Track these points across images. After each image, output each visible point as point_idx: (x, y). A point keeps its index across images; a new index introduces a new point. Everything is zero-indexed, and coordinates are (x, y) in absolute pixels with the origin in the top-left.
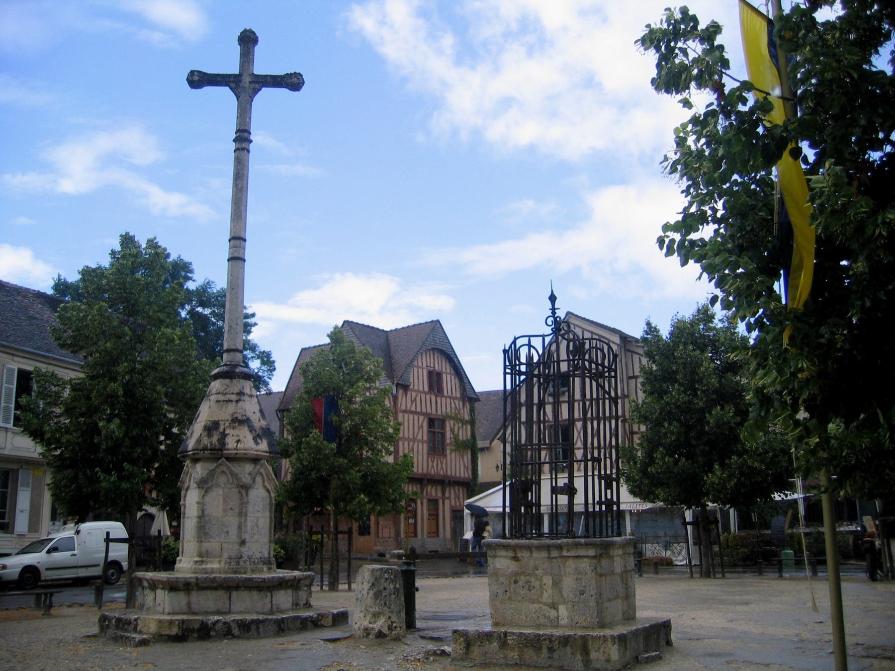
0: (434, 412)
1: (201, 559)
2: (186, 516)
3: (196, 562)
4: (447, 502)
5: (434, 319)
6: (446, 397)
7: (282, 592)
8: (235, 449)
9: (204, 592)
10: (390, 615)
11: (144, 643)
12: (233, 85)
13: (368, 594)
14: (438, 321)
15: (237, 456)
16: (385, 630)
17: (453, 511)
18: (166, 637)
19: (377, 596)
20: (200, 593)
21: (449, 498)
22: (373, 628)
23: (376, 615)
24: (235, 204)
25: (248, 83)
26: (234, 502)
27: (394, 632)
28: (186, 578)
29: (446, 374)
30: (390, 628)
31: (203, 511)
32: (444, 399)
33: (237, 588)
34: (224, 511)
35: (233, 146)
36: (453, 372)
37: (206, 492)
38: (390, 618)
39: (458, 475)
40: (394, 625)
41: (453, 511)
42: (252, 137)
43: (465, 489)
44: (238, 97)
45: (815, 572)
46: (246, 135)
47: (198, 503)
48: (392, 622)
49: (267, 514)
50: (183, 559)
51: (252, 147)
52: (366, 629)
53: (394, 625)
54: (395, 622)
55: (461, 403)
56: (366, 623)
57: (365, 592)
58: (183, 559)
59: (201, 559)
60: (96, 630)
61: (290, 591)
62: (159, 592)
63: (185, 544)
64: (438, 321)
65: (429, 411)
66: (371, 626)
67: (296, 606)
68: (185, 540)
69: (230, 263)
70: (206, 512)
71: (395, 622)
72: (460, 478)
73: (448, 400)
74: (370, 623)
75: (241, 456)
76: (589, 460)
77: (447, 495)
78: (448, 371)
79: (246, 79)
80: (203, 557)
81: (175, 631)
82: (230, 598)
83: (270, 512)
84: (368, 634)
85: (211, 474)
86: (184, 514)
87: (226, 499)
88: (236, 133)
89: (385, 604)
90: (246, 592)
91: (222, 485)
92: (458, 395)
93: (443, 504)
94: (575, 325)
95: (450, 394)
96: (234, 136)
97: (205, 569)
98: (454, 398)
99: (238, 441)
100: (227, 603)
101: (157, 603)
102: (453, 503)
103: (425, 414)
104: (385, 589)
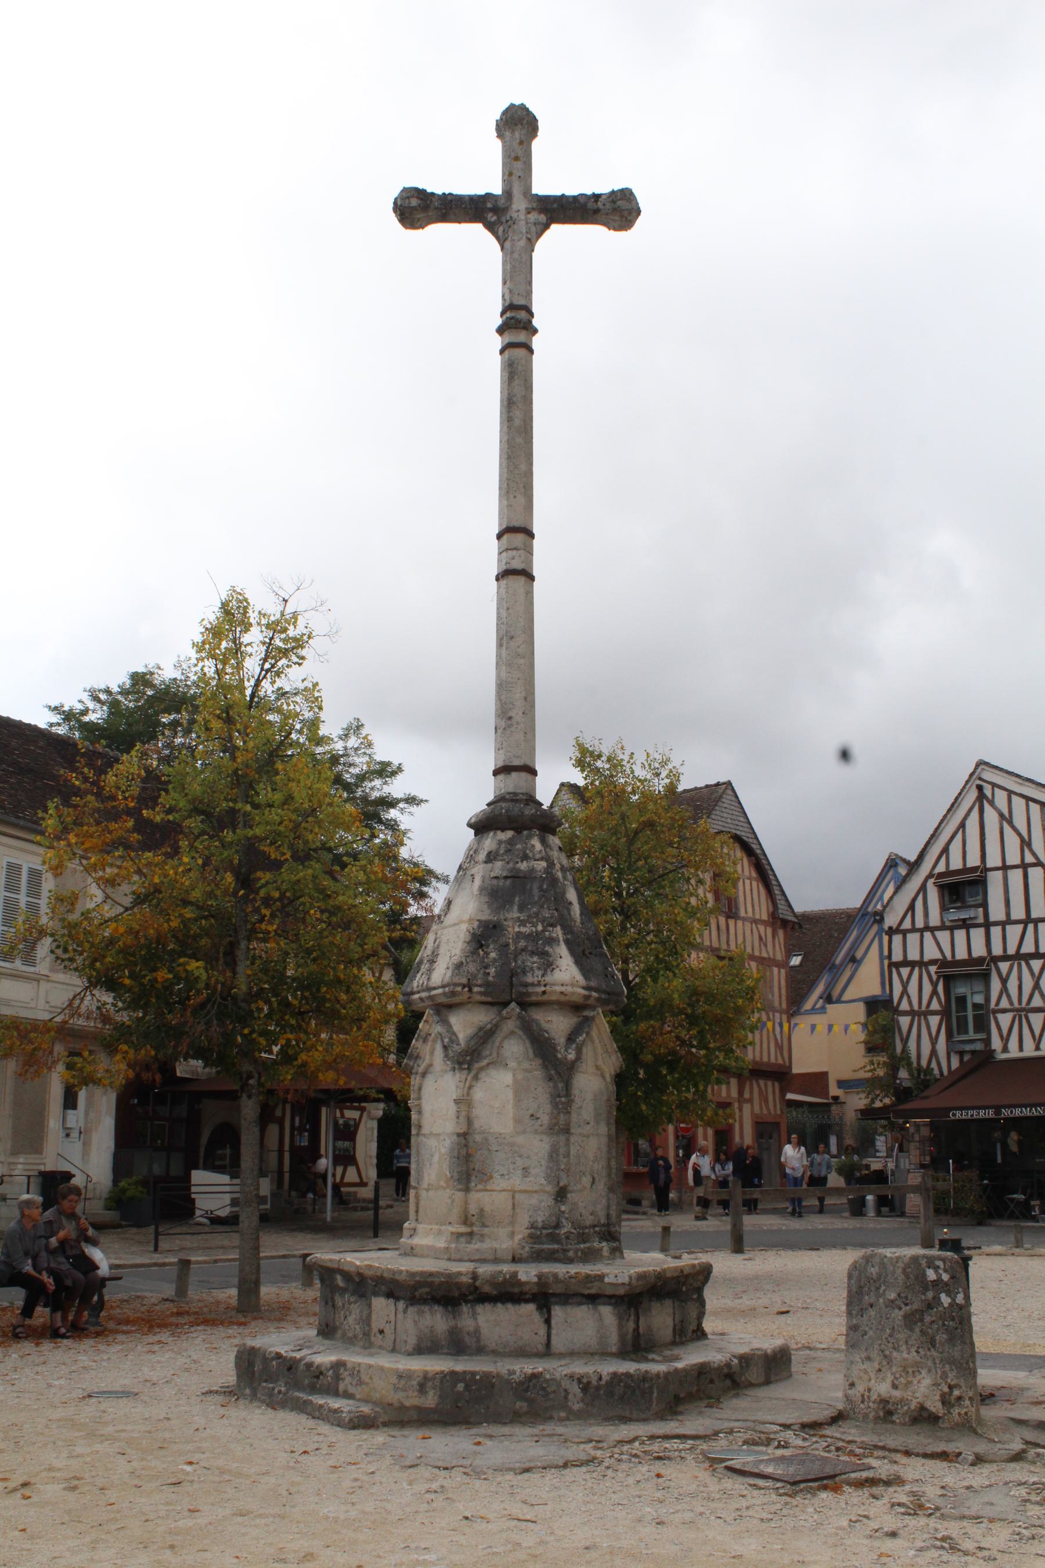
0: (724, 946)
2: (425, 1131)
3: (459, 1235)
4: (747, 1108)
5: (722, 780)
6: (744, 919)
7: (656, 1306)
11: (362, 1423)
12: (492, 217)
14: (729, 784)
16: (935, 1405)
17: (756, 1123)
20: (479, 1308)
21: (750, 1101)
22: (902, 1401)
24: (509, 458)
25: (523, 212)
26: (540, 1099)
27: (956, 1411)
28: (450, 1276)
29: (750, 878)
30: (945, 1401)
31: (469, 1121)
32: (740, 923)
34: (517, 1121)
35: (497, 342)
36: (754, 874)
37: (476, 1078)
39: (765, 1059)
40: (956, 1392)
41: (756, 1123)
42: (535, 322)
43: (777, 1085)
44: (502, 241)
46: (522, 315)
47: (457, 1102)
48: (950, 1387)
49: (603, 1129)
50: (421, 1227)
51: (536, 342)
52: (884, 1402)
53: (956, 1392)
54: (956, 1386)
55: (769, 930)
58: (421, 1227)
60: (230, 1377)
61: (668, 1302)
62: (380, 1304)
63: (423, 1194)
64: (729, 784)
65: (715, 944)
66: (897, 1394)
67: (680, 1335)
68: (425, 1185)
69: (503, 582)
70: (477, 1124)
71: (956, 1386)
72: (768, 1064)
73: (748, 925)
74: (895, 1387)
75: (554, 998)
77: (747, 1095)
78: (747, 873)
79: (519, 204)
80: (472, 1225)
81: (430, 1400)
82: (548, 1321)
83: (608, 1124)
84: (890, 1413)
85: (485, 1036)
86: (420, 1127)
87: (519, 1091)
88: (502, 314)
90: (584, 1308)
91: (512, 1064)
92: (765, 917)
93: (741, 1110)
94: (994, 785)
95: (750, 914)
96: (499, 321)
98: (755, 921)
100: (542, 1331)
101: (376, 1325)
102: (757, 1110)
104: (930, 1306)
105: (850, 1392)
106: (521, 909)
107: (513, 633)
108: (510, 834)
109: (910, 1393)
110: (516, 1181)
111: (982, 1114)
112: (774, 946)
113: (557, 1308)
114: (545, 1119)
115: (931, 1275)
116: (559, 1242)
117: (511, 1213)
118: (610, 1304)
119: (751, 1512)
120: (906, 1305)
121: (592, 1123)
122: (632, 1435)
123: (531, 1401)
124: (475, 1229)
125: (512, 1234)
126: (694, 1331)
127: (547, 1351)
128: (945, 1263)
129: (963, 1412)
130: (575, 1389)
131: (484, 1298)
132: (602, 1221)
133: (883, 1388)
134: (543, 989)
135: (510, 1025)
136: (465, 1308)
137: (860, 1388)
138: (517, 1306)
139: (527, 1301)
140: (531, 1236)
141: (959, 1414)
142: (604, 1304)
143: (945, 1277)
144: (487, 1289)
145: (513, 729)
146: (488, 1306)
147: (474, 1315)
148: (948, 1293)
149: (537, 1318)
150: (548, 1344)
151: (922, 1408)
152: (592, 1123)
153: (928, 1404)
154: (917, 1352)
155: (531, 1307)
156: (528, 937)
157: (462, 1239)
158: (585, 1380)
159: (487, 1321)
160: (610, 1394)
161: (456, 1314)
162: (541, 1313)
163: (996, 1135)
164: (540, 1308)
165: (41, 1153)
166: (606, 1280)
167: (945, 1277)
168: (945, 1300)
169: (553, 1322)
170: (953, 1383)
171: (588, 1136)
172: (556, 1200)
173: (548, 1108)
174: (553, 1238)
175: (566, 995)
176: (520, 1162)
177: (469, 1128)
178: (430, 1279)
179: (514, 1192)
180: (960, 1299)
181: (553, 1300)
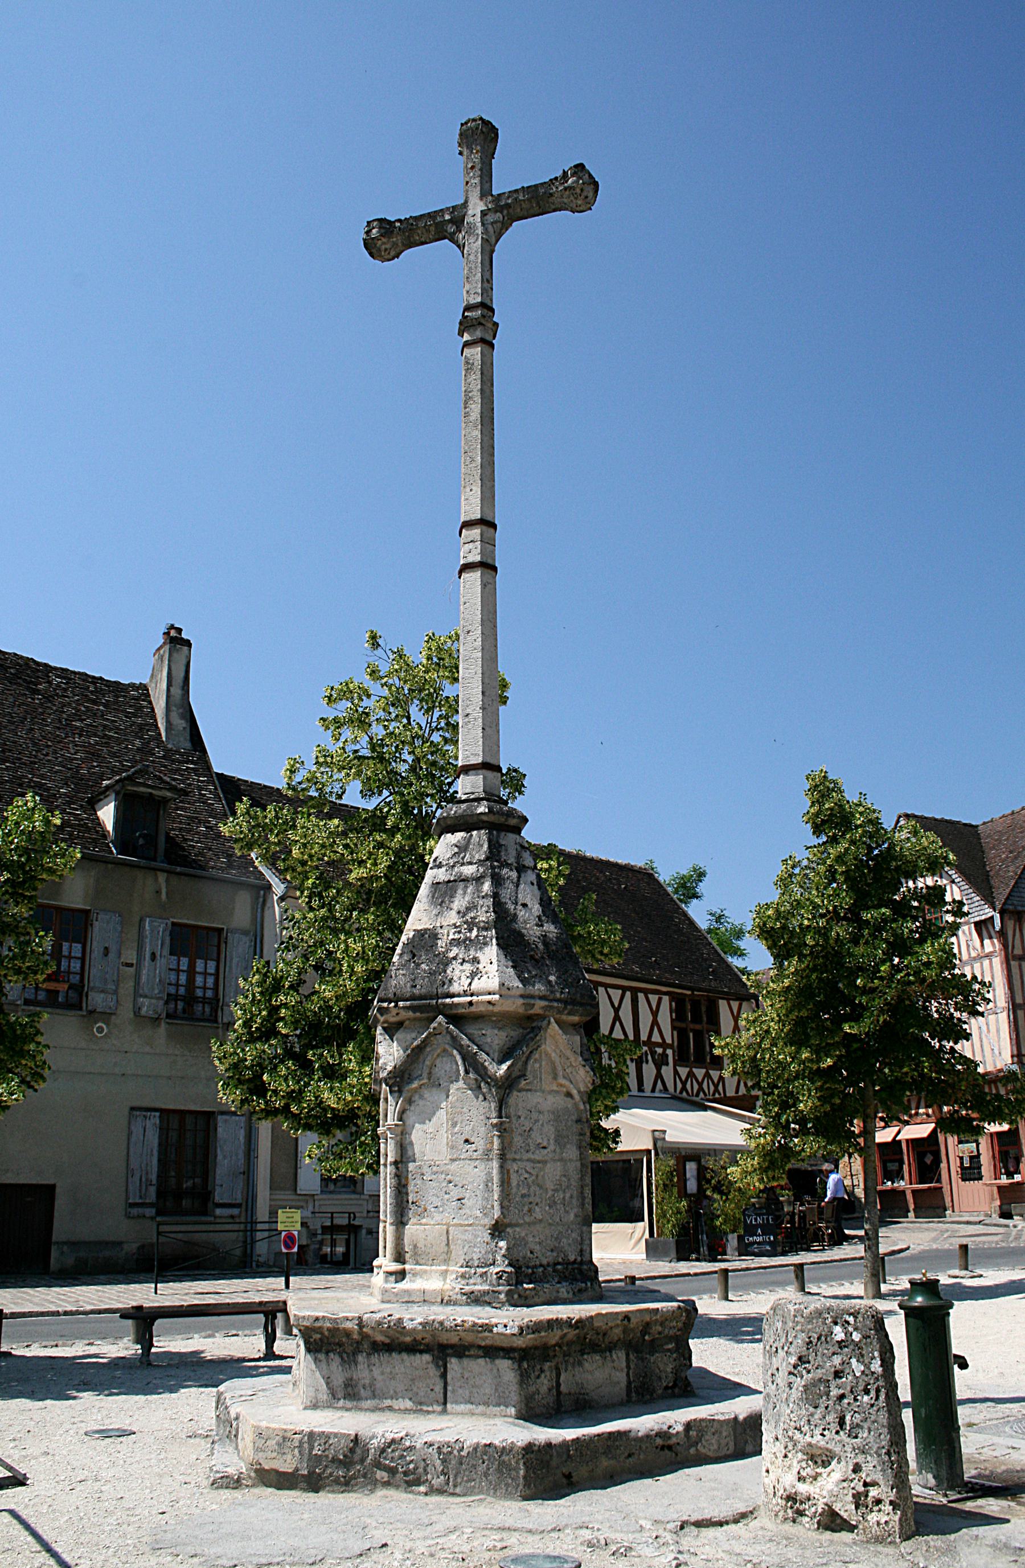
1: (400, 1267)
8: (465, 994)
9: (385, 1357)
10: (860, 1459)
13: (790, 1385)
15: (473, 1009)
16: (846, 1509)
18: (273, 1477)
19: (813, 1394)
20: (374, 1358)
23: (821, 1458)
27: (873, 1518)
30: (859, 1500)
33: (461, 1350)
37: (410, 1101)
38: (857, 1469)
45: (494, 1126)
54: (874, 1484)
56: (789, 1480)
57: (782, 1378)
59: (400, 1267)
71: (874, 1484)
74: (801, 1479)
76: (906, 1404)
82: (444, 1376)
89: (842, 1422)
90: (481, 1361)
97: (407, 1292)
99: (473, 975)
103: (466, 202)
104: (838, 1374)
107: (469, 628)
108: (460, 835)
109: (818, 1490)
112: (1014, 935)
113: (454, 1360)
117: (446, 1249)
118: (509, 1358)
120: (809, 1372)
121: (552, 1147)
124: (407, 1267)
126: (667, 1388)
128: (856, 1317)
129: (883, 1521)
132: (572, 1258)
134: (469, 999)
135: (443, 1041)
138: (412, 1357)
139: (421, 1352)
141: (878, 1524)
142: (504, 1358)
143: (856, 1337)
144: (380, 1338)
145: (470, 726)
148: (860, 1358)
149: (434, 1372)
152: (552, 1147)
153: (837, 1507)
154: (822, 1435)
155: (427, 1357)
157: (392, 1278)
158: (445, 1450)
159: (382, 1373)
162: (437, 1366)
164: (435, 1361)
165: (50, 1190)
166: (495, 1329)
167: (856, 1337)
168: (857, 1367)
169: (449, 1377)
170: (868, 1480)
171: (545, 1162)
172: (492, 1235)
175: (494, 1005)
176: (455, 1193)
177: (402, 1156)
178: (317, 1324)
179: (448, 1225)
181: (450, 1351)
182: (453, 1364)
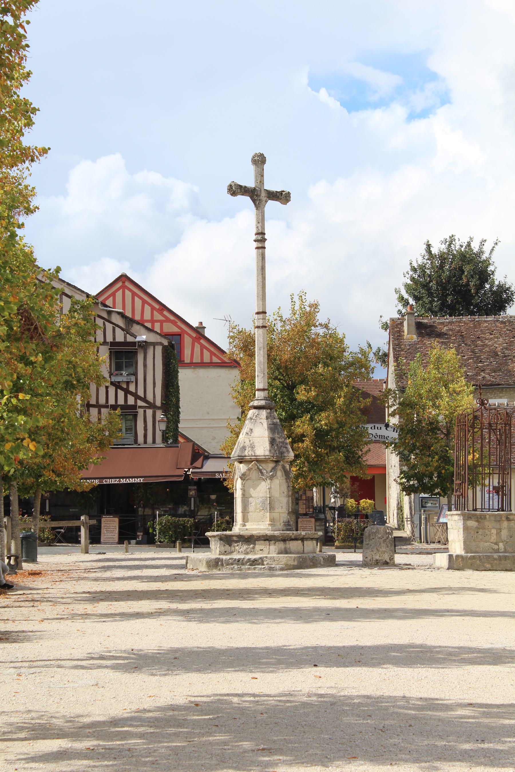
16: (388, 561)
30: (390, 560)
66: (380, 558)
79: (263, 195)
81: (296, 563)
82: (303, 545)
84: (377, 563)
91: (279, 478)
105: (366, 559)
106: (278, 434)
110: (280, 510)
111: (138, 480)
114: (286, 493)
115: (388, 531)
116: (290, 526)
119: (9, 750)
122: (34, 671)
123: (313, 562)
125: (280, 524)
127: (303, 553)
130: (322, 559)
131: (292, 540)
133: (377, 557)
136: (287, 542)
137: (369, 558)
140: (284, 525)
146: (292, 541)
147: (289, 544)
149: (301, 544)
150: (304, 551)
151: (386, 561)
155: (300, 541)
156: (281, 442)
160: (328, 560)
161: (285, 544)
163: (191, 493)
173: (286, 490)
174: (289, 525)
180: (337, 543)
182: (305, 542)
